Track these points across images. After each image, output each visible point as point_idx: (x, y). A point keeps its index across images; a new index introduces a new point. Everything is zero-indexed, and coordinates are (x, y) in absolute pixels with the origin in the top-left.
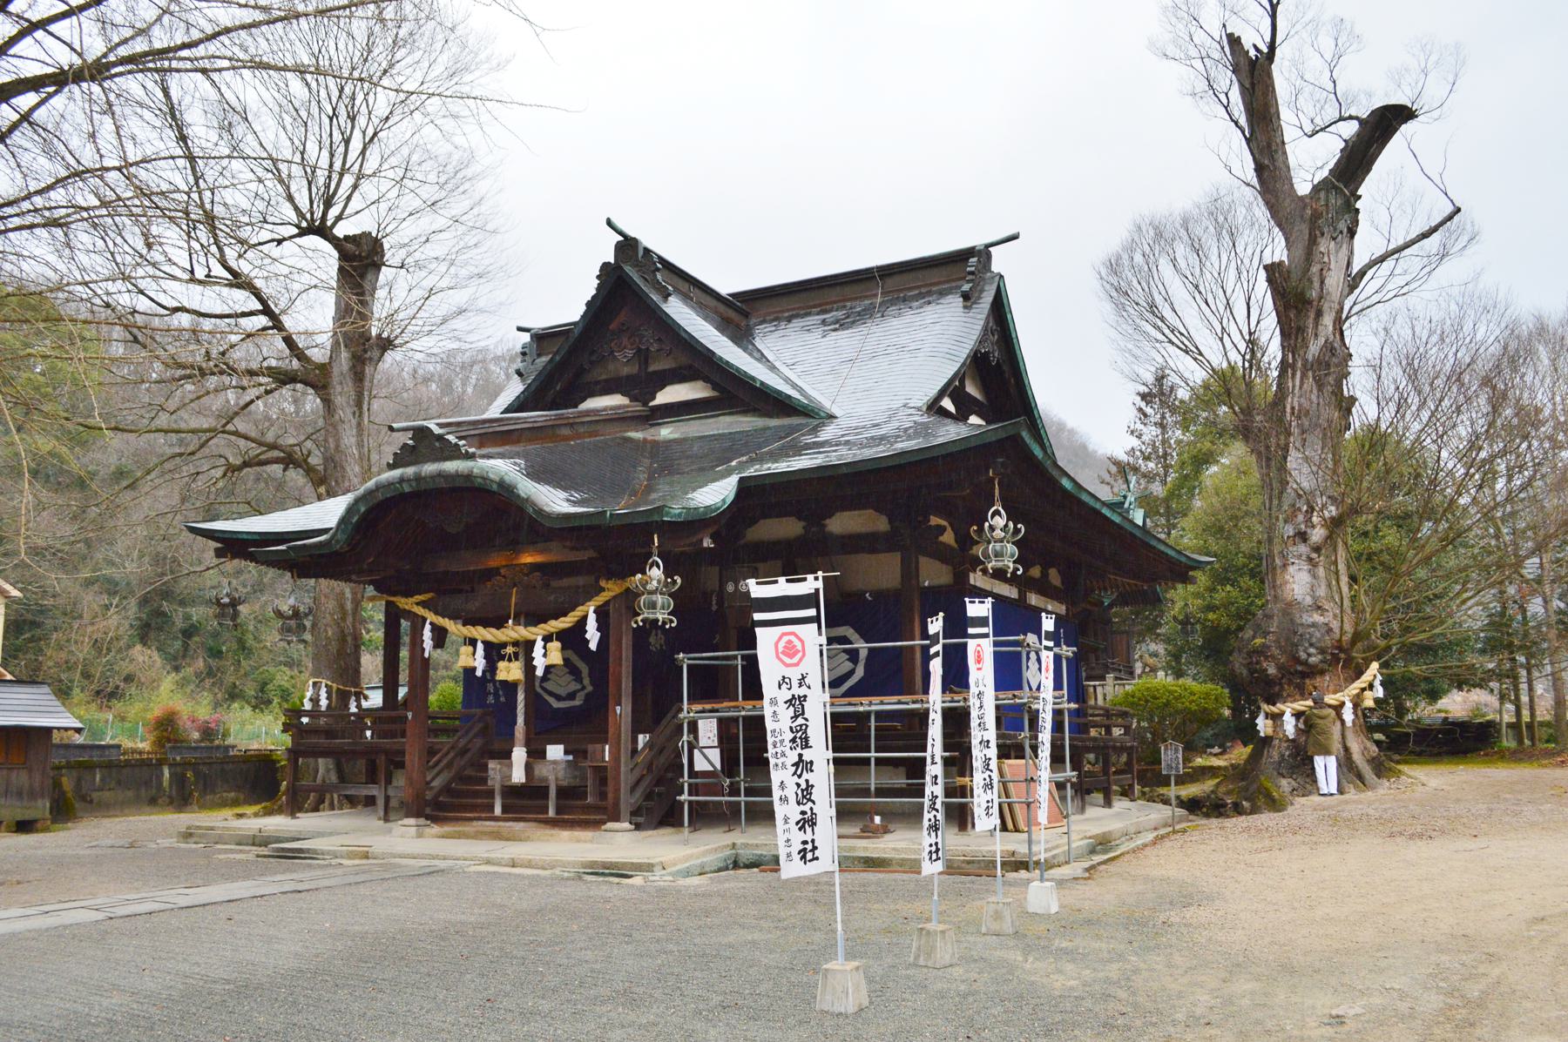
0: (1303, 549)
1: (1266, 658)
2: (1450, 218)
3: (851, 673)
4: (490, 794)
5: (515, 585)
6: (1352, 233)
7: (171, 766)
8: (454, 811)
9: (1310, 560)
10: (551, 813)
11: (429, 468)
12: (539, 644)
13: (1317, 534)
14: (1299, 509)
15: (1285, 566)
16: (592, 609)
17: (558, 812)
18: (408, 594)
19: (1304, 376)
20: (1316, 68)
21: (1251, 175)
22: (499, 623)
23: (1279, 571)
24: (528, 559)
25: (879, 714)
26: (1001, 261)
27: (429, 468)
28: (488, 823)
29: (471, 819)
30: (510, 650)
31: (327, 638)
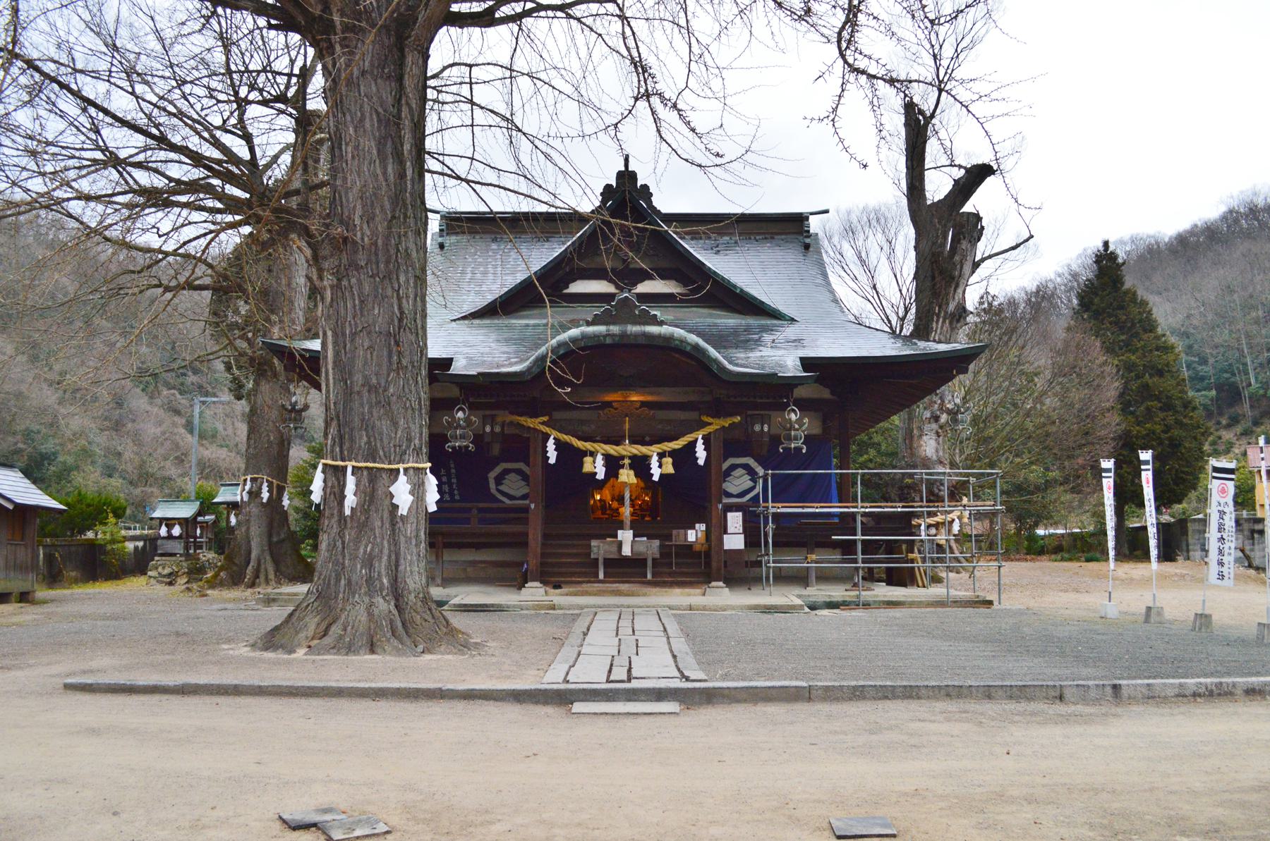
0: (934, 426)
1: (915, 491)
5: (626, 416)
7: (45, 547)
8: (571, 577)
9: (937, 433)
10: (649, 576)
14: (935, 402)
15: (921, 436)
16: (700, 437)
17: (654, 575)
18: (535, 415)
19: (944, 322)
23: (916, 438)
24: (634, 399)
25: (864, 515)
26: (815, 224)
28: (596, 585)
29: (583, 582)
31: (269, 442)
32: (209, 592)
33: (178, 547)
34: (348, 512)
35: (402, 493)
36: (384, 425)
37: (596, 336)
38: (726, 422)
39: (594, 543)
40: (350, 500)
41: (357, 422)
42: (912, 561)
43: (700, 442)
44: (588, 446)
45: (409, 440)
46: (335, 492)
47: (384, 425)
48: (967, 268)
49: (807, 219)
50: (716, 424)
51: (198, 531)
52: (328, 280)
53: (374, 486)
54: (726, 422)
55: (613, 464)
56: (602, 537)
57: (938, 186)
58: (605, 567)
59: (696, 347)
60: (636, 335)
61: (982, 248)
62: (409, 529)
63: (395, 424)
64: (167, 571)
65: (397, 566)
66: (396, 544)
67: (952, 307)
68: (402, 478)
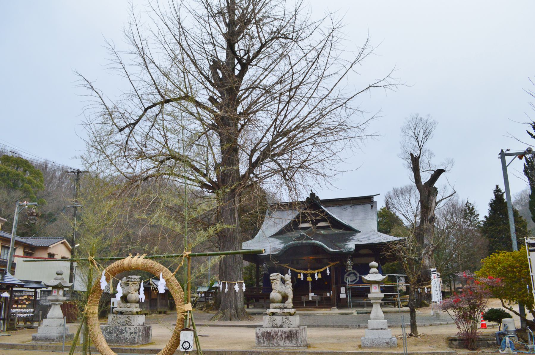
2: (454, 193)
3: (356, 279)
4: (303, 302)
6: (436, 195)
7: (170, 300)
10: (317, 306)
11: (304, 242)
12: (316, 274)
13: (430, 253)
17: (318, 305)
20: (426, 161)
21: (414, 181)
22: (307, 270)
24: (311, 258)
26: (375, 199)
27: (308, 241)
30: (309, 275)
32: (210, 312)
33: (203, 300)
34: (226, 292)
35: (237, 288)
36: (233, 274)
37: (295, 244)
38: (334, 264)
39: (302, 297)
40: (226, 289)
41: (228, 273)
42: (394, 300)
43: (328, 269)
44: (299, 271)
45: (238, 276)
46: (224, 288)
47: (233, 274)
48: (433, 204)
49: (373, 197)
50: (332, 264)
51: (210, 295)
52: (222, 244)
53: (231, 286)
54: (334, 264)
55: (305, 276)
56: (305, 295)
57: (425, 177)
58: (305, 303)
59: (321, 245)
60: (305, 243)
61: (439, 197)
62: (239, 295)
63: (235, 273)
64: (201, 306)
65: (236, 303)
66: (236, 298)
67: (429, 217)
68: (237, 285)
